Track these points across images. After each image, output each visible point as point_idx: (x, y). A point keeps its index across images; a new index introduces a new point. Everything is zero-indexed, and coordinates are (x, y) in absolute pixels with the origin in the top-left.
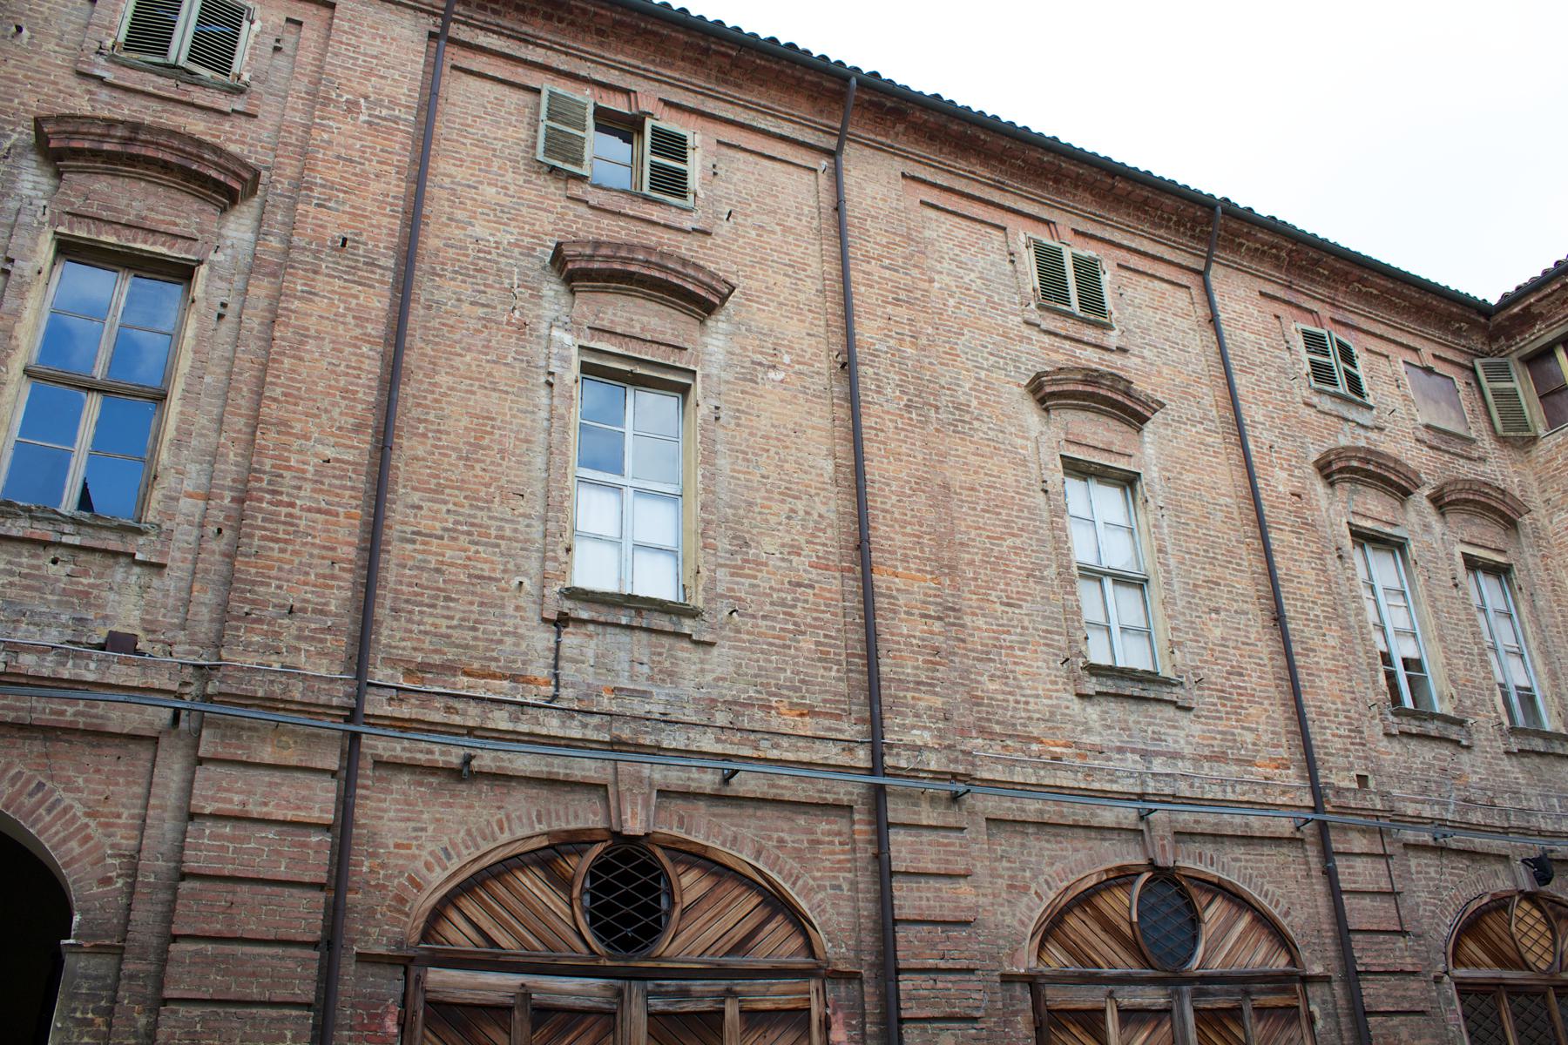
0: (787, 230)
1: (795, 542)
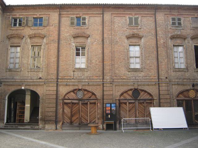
0: (97, 25)
1: (96, 60)
